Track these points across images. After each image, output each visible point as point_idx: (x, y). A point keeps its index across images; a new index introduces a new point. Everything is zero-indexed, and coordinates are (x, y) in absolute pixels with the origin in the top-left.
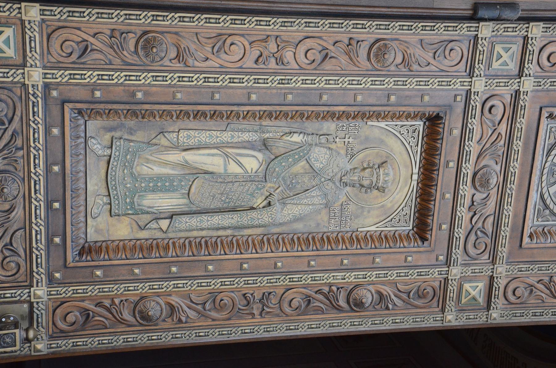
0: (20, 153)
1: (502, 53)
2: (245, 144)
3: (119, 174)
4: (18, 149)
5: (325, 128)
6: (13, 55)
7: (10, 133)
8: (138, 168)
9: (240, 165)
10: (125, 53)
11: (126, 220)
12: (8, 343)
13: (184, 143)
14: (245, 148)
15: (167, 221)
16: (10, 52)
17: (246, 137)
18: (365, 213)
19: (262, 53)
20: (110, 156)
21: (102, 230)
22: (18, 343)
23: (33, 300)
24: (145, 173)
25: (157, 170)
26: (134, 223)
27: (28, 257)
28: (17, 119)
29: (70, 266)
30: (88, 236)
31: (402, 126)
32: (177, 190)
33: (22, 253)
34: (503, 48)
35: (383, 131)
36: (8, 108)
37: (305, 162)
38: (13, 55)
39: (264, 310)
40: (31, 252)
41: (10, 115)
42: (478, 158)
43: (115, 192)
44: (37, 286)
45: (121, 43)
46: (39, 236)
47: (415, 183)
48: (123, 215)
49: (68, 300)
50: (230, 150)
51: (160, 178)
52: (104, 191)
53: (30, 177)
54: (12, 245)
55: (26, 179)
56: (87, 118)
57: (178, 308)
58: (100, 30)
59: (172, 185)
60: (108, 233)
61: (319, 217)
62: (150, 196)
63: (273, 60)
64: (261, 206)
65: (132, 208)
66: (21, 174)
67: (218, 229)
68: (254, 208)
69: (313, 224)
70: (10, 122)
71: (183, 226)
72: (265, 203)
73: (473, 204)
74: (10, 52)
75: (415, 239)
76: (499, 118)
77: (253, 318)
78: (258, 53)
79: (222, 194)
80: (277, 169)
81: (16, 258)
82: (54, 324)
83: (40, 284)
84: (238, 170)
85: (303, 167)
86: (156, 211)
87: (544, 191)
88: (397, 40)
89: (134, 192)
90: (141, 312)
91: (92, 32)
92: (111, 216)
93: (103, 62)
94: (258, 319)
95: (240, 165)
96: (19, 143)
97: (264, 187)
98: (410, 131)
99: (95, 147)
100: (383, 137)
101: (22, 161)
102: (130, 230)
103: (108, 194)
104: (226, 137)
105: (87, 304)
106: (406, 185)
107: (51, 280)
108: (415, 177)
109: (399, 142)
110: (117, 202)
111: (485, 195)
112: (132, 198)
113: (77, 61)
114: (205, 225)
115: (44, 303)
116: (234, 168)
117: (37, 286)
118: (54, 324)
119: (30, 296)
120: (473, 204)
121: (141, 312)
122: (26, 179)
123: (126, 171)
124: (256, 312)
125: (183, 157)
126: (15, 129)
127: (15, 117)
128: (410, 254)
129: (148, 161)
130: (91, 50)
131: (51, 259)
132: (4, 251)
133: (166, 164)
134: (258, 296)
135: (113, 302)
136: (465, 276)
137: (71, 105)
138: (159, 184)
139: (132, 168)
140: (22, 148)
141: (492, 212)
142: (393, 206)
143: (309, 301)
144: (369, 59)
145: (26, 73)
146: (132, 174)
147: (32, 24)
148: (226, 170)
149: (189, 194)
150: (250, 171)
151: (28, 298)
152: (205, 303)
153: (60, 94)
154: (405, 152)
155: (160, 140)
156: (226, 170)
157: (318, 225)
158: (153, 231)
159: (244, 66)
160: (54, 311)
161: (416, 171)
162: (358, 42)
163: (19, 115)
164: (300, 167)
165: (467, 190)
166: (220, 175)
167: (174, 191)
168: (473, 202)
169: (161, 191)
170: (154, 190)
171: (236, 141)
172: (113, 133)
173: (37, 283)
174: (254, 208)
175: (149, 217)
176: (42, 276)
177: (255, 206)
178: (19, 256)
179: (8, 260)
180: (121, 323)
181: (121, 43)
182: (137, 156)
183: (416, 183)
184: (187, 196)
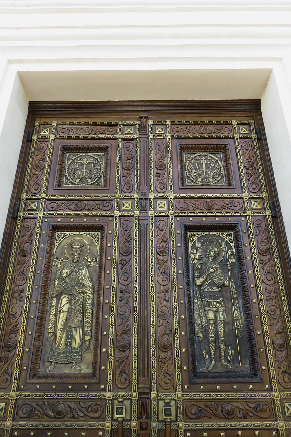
0: (46, 403)
1: (125, 206)
2: (57, 304)
3: (62, 359)
4: (44, 404)
5: (54, 271)
6: (4, 404)
7: (37, 407)
8: (61, 350)
9: (65, 305)
10: (9, 356)
11: (85, 355)
12: (121, 411)
13: (53, 330)
14: (58, 304)
15: (86, 337)
16: (286, 405)
17: (54, 303)
18: (92, 251)
19: (164, 300)
20: (55, 362)
21: (87, 366)
22: (122, 406)
23: (157, 399)
24: (63, 347)
25: (63, 342)
26: (86, 351)
27: (93, 400)
28: (31, 403)
29: (98, 381)
30: (89, 372)
31: (190, 240)
32: (72, 333)
33: (90, 403)
34: (158, 206)
35: (58, 247)
36: (26, 407)
37: (67, 278)
38: (4, 404)
39: (273, 292)
40: (89, 399)
41: (29, 406)
42: (71, 210)
43: (70, 360)
44: (105, 396)
45: (6, 358)
46: (230, 395)
47: (81, 233)
48: (82, 357)
49: (158, 382)
50: (58, 310)
51: (66, 340)
52: (70, 365)
53: (56, 399)
54: (87, 407)
55: (57, 400)
56: (37, 373)
57: (277, 331)
58: (277, 366)
59: (70, 335)
60: (89, 363)
61: (92, 270)
62: (74, 344)
63: (166, 295)
64: (83, 295)
65: (79, 352)
66: (55, 402)
67: (92, 314)
68: (84, 299)
69: (94, 273)
70: (33, 407)
71: (89, 329)
72: (82, 294)
73: (219, 209)
74: (286, 405)
75: (236, 230)
76: (56, 204)
77: (131, 297)
78: (164, 301)
79: (76, 313)
80: (68, 290)
81: (93, 406)
82: (125, 388)
83: (105, 395)
84: (67, 306)
85: (68, 279)
86: (81, 342)
87: (212, 183)
88: (20, 246)
89: (71, 352)
90: (280, 348)
91: (279, 370)
92: (81, 362)
93: (172, 366)
94: (131, 294)
95: (65, 305)
96: (41, 403)
97: (75, 295)
98: (192, 236)
99: (50, 369)
100: (61, 247)
101: (50, 402)
102: (89, 353)
103: (72, 364)
104: (53, 312)
105: (118, 373)
106: (82, 236)
107: (270, 390)
108: (78, 233)
109: (64, 241)
110: (75, 359)
111: (215, 205)
112: (74, 353)
113: (10, 377)
114: (90, 320)
115: (114, 393)
116: (65, 308)
117: (105, 396)
118: (125, 388)
119: (110, 400)
120: (219, 209)
121: (280, 348)
122: (57, 400)
123: (61, 355)
124: (128, 295)
125: (59, 330)
126: (36, 405)
127: (30, 404)
128: (242, 232)
129: (59, 346)
130: (7, 371)
131: (95, 390)
132: (257, 411)
133: (61, 338)
134: (121, 295)
135: (118, 361)
136: (250, 209)
137: (28, 380)
138: (69, 340)
139: (61, 353)
140: (44, 402)
141: (94, 202)
142: (90, 240)
143: (268, 272)
144: (165, 256)
145: (134, 398)
146: (63, 353)
147: (159, 396)
148: (66, 312)
149: (74, 327)
150: (68, 301)
151: (111, 400)
152: (274, 319)
153: (22, 384)
154: (68, 238)
155: (51, 340)
156: (66, 312)
157: (95, 271)
158: (91, 343)
159: (170, 306)
160: (120, 388)
161: (76, 233)
162: (158, 261)
163: (29, 402)
164: (68, 280)
165: (215, 212)
166: (68, 314)
167: (72, 334)
168: (218, 209)
169: (72, 340)
170: (71, 342)
171: (55, 308)
172: (46, 361)
173: (104, 396)
174: (84, 299)
175: (84, 345)
176: (101, 394)
177: (83, 298)
178: (92, 404)
179: (93, 409)
180: (286, 357)
181: (6, 358)
182: (56, 350)
183: (81, 232)
184: (76, 328)
